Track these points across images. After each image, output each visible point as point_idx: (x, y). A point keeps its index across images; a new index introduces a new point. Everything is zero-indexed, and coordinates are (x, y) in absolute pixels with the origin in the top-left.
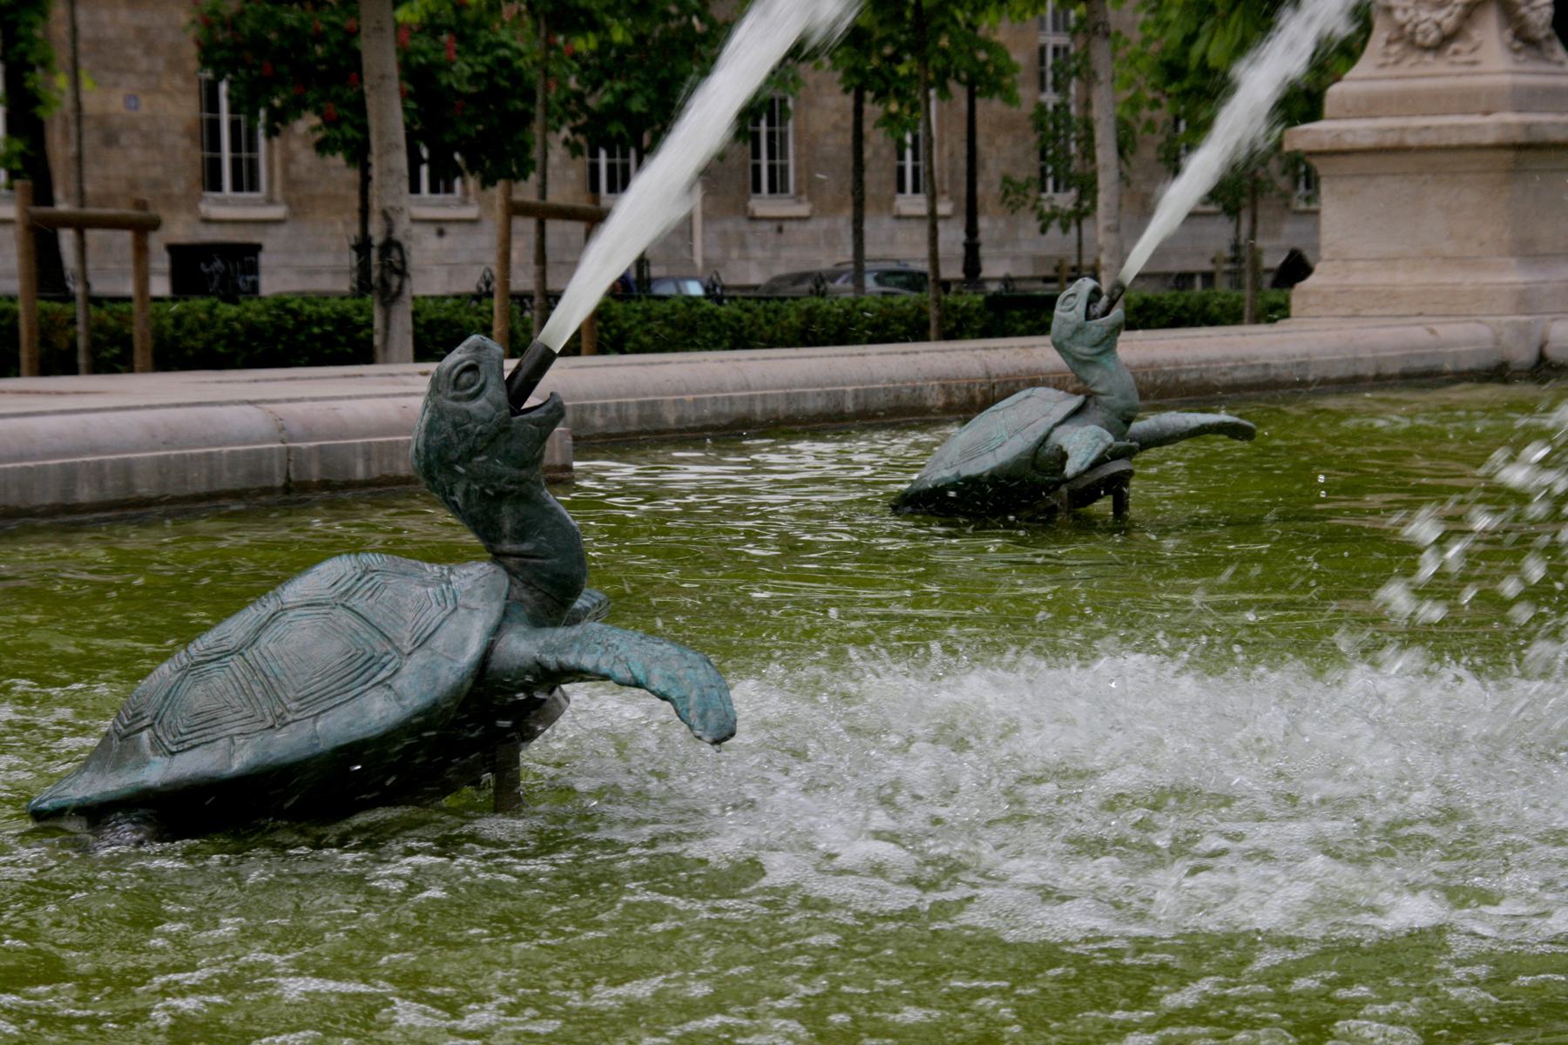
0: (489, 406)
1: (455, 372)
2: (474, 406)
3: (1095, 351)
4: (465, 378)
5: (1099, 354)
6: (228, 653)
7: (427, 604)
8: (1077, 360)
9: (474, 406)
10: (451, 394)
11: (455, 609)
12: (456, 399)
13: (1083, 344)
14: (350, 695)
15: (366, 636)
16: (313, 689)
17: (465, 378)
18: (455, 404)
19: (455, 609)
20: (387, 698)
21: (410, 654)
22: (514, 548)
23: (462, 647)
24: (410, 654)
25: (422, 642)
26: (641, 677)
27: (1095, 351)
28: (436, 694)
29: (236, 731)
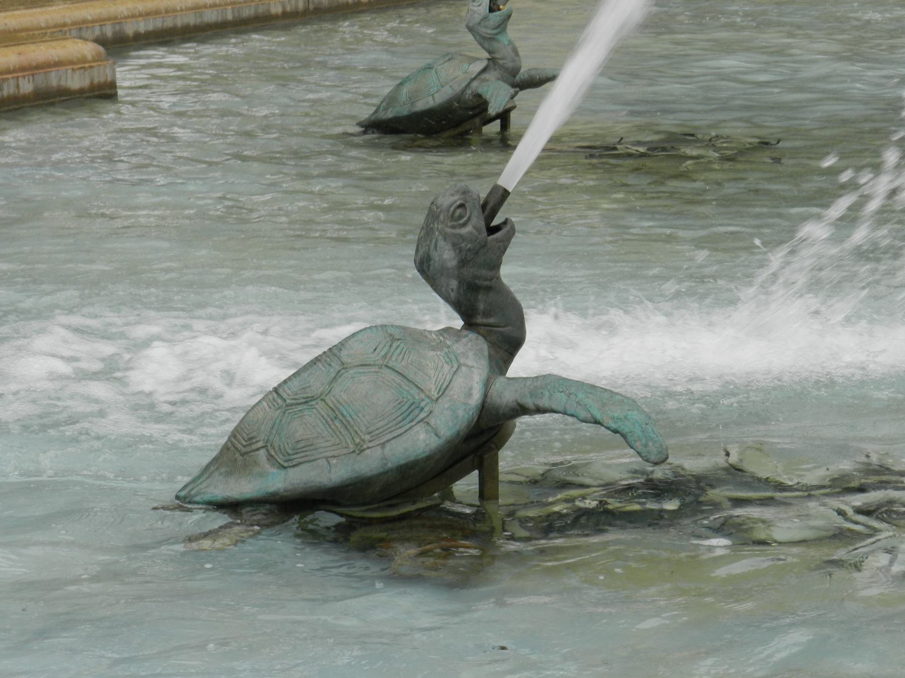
0: (474, 231)
1: (452, 209)
2: (464, 231)
3: (495, 32)
4: (458, 212)
5: (497, 34)
6: (313, 399)
7: (440, 364)
8: (484, 38)
9: (464, 231)
10: (449, 224)
11: (459, 367)
12: (453, 227)
13: (486, 27)
14: (403, 429)
15: (407, 388)
16: (378, 425)
17: (458, 212)
18: (454, 231)
19: (459, 367)
20: (427, 432)
21: (437, 399)
22: (485, 321)
23: (469, 395)
24: (437, 399)
25: (443, 391)
26: (598, 416)
27: (495, 32)
28: (457, 427)
29: (332, 453)
